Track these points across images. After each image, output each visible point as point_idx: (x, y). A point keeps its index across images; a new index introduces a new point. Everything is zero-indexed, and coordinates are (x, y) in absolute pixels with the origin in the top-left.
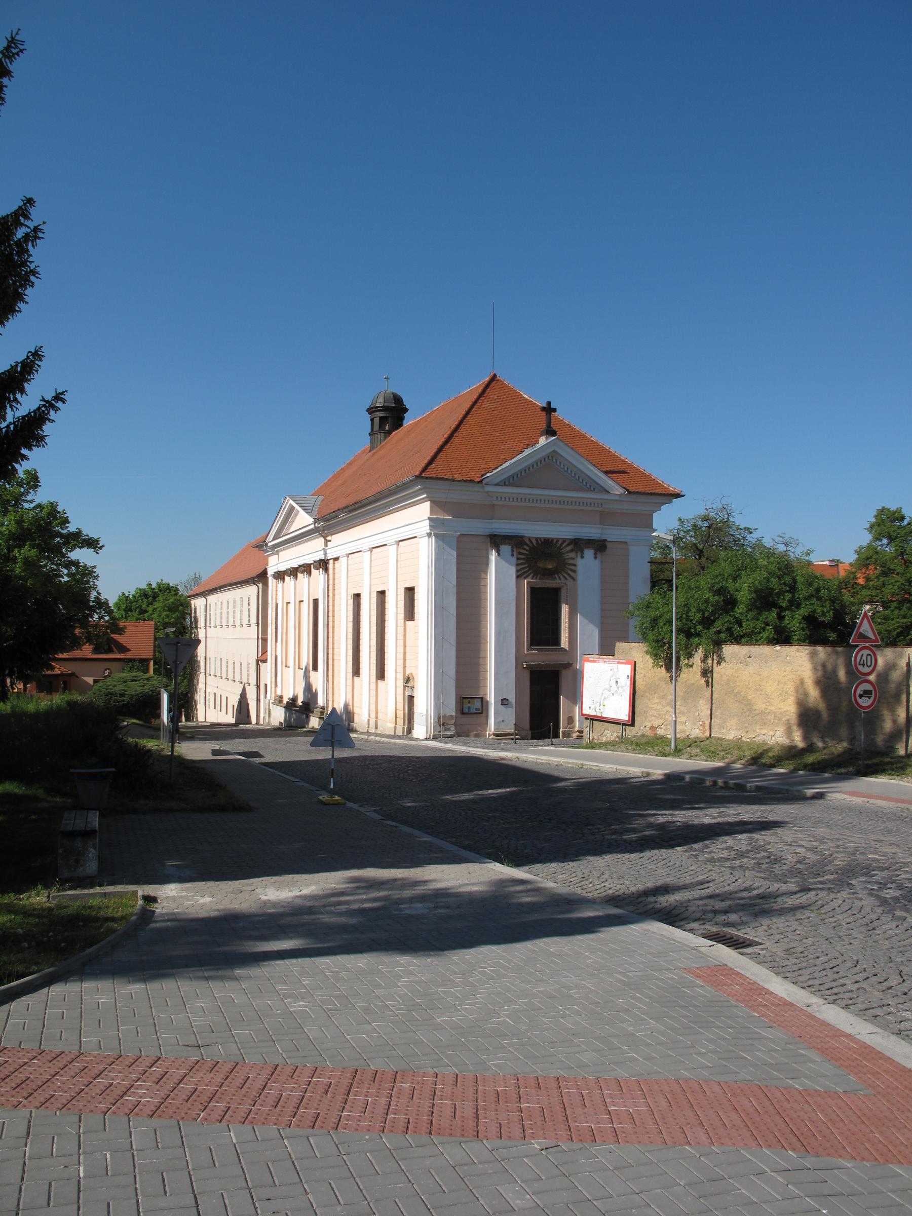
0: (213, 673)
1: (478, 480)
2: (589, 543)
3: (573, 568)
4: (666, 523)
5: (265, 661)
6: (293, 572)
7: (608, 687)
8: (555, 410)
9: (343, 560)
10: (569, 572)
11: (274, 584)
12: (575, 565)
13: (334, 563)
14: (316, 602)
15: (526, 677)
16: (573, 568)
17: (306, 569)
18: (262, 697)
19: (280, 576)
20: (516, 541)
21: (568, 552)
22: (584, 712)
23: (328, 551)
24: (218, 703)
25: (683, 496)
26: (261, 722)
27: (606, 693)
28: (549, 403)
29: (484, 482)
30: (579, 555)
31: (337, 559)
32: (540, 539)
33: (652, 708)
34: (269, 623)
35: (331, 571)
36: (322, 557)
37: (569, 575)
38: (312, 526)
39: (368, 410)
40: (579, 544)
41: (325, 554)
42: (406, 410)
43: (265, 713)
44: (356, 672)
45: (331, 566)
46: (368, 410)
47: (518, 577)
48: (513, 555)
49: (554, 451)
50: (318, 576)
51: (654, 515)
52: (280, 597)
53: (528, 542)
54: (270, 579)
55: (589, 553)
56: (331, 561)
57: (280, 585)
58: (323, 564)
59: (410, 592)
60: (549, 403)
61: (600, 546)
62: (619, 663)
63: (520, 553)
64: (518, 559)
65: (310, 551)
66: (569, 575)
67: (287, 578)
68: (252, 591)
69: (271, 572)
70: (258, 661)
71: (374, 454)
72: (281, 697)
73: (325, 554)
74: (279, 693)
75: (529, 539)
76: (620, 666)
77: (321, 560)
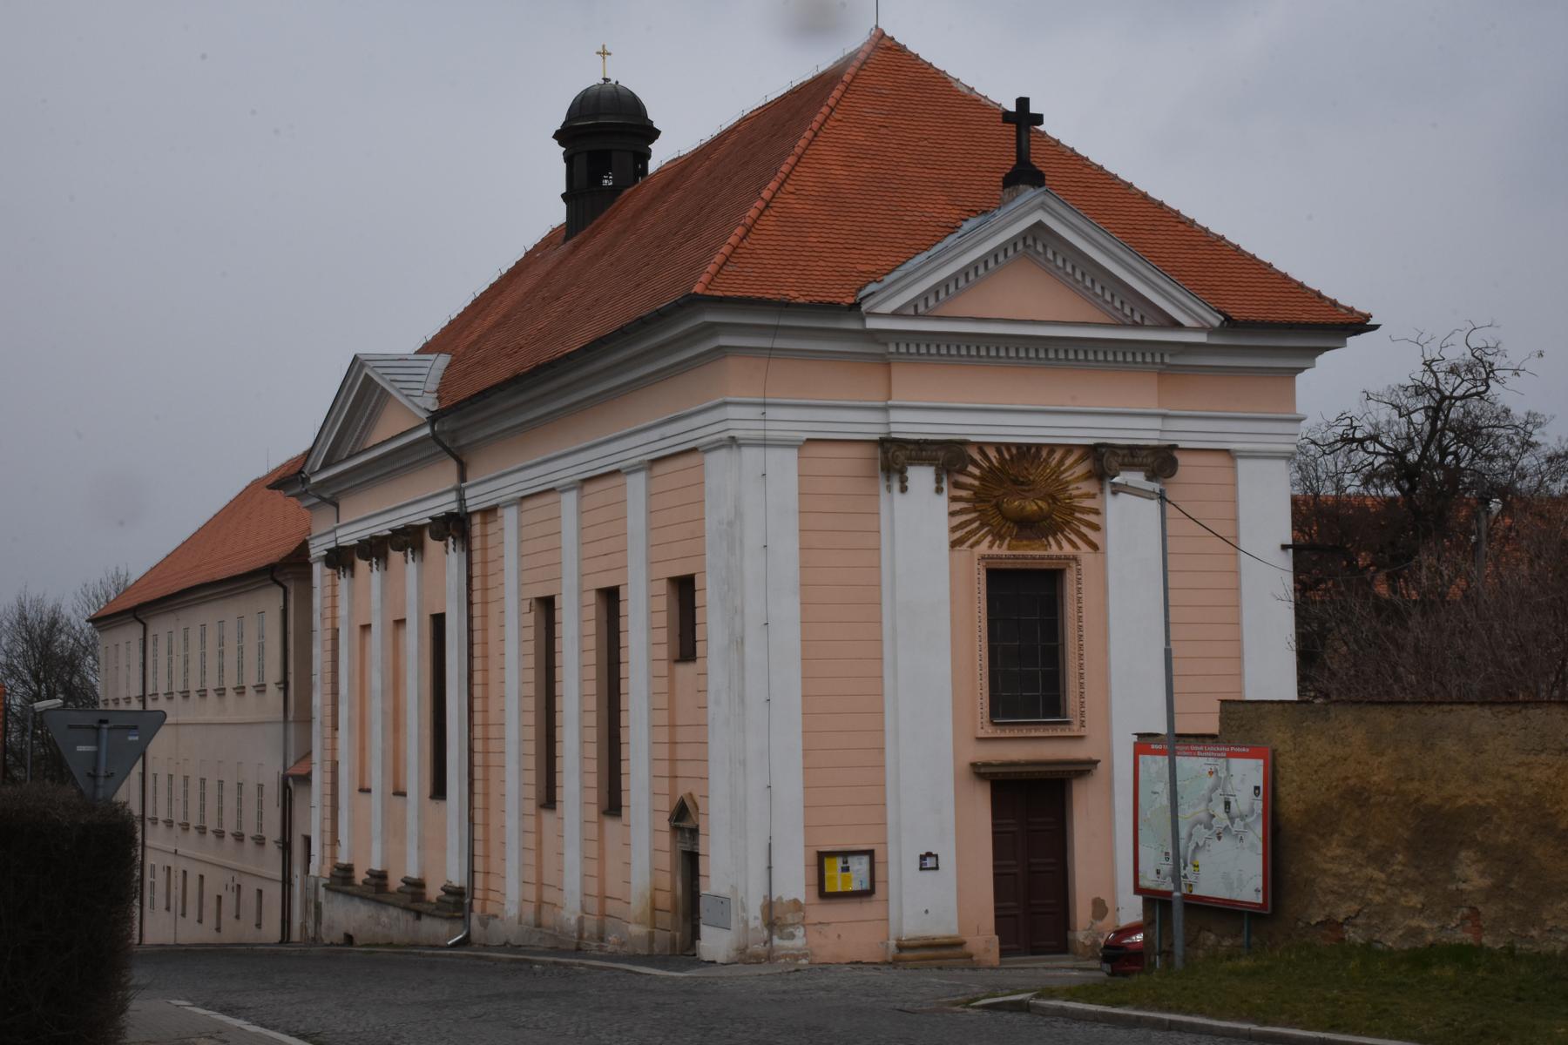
0: (162, 815)
1: (851, 300)
2: (1132, 456)
3: (1092, 518)
4: (1340, 390)
5: (306, 779)
6: (375, 549)
7: (1203, 816)
8: (1039, 119)
9: (509, 517)
10: (1084, 530)
11: (328, 580)
12: (1097, 512)
13: (484, 523)
14: (439, 621)
15: (981, 802)
16: (1092, 518)
17: (409, 539)
18: (297, 871)
19: (340, 559)
20: (948, 457)
21: (1078, 479)
22: (1144, 883)
23: (468, 494)
24: (176, 892)
25: (1376, 327)
26: (296, 935)
27: (1201, 833)
28: (1023, 103)
29: (864, 308)
30: (896, 486)
31: (490, 512)
32: (1008, 446)
33: (1324, 871)
34: (316, 679)
35: (476, 544)
36: (454, 507)
37: (1084, 537)
38: (426, 431)
39: (560, 136)
40: (1103, 461)
41: (461, 500)
42: (654, 134)
43: (306, 911)
44: (548, 799)
45: (476, 530)
46: (560, 136)
47: (954, 544)
48: (939, 490)
49: (1039, 225)
50: (446, 560)
51: (557, 214)
52: (343, 611)
53: (977, 457)
54: (318, 570)
55: (921, 477)
56: (477, 520)
57: (343, 583)
58: (455, 527)
59: (610, 598)
60: (1023, 103)
61: (1160, 462)
62: (1231, 755)
63: (957, 485)
64: (953, 499)
65: (425, 496)
66: (1084, 537)
67: (361, 565)
68: (269, 603)
69: (318, 549)
70: (285, 779)
71: (576, 247)
72: (348, 870)
73: (461, 500)
74: (343, 859)
75: (981, 447)
76: (1235, 762)
77: (449, 516)
